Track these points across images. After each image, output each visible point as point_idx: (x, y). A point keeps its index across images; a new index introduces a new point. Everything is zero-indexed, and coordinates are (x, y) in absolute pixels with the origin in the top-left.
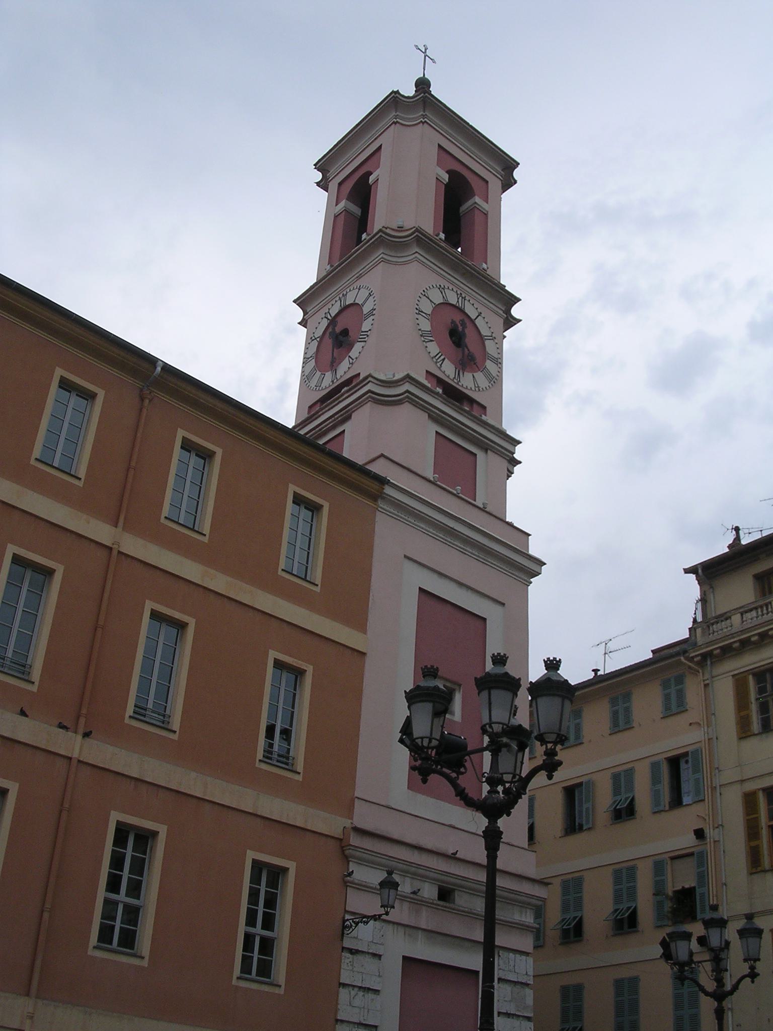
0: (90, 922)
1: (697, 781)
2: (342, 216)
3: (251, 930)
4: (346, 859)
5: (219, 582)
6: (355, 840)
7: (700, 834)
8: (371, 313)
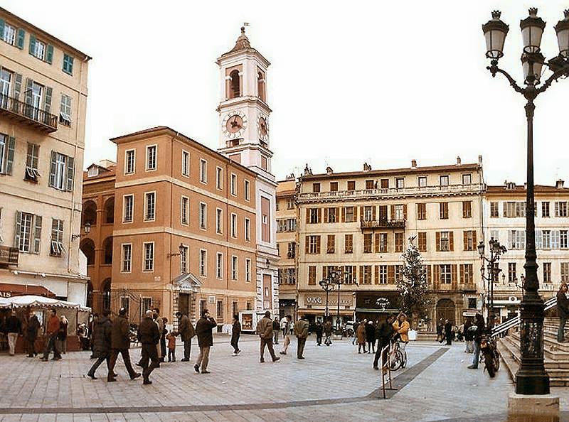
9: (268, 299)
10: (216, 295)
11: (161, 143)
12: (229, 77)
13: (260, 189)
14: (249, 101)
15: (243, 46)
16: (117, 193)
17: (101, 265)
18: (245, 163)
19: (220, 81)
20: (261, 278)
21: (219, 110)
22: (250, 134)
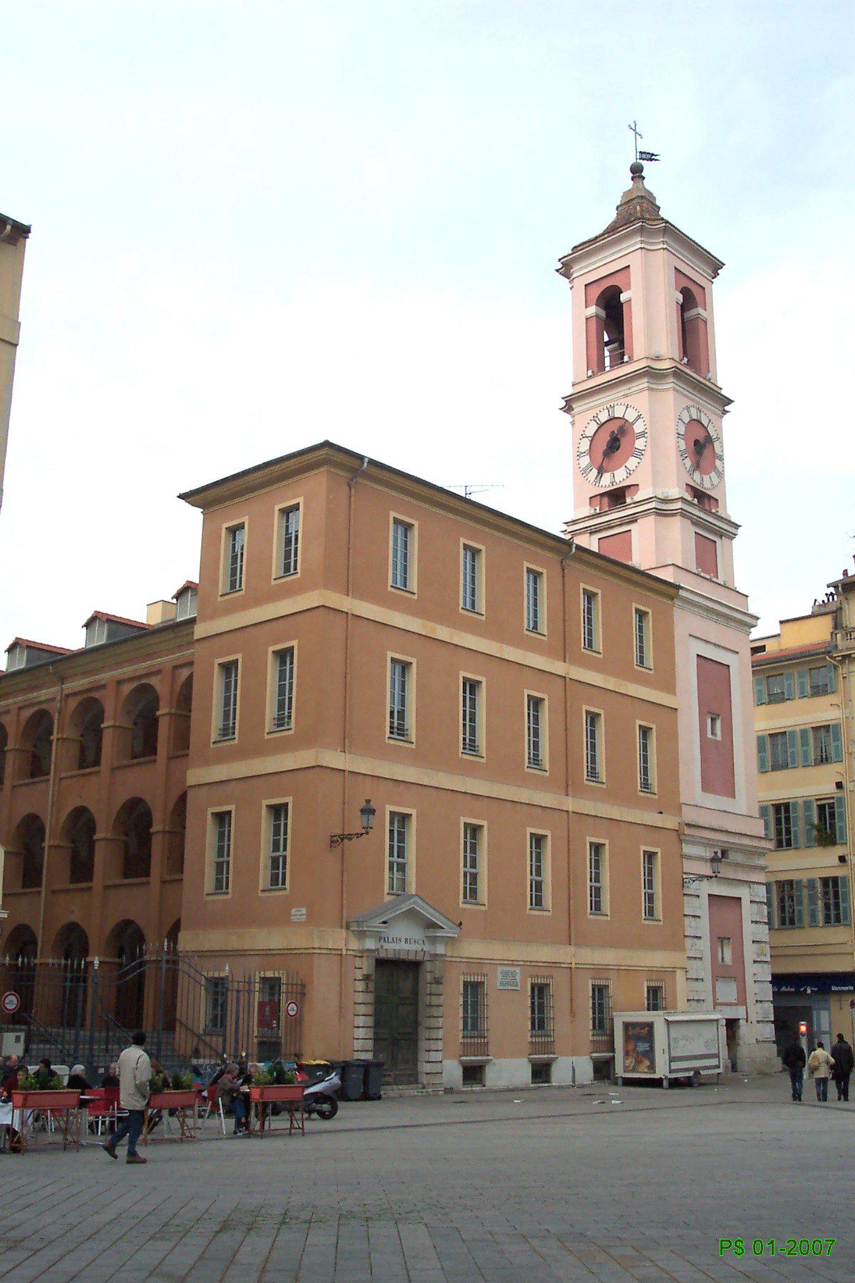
0: (383, 882)
1: (836, 747)
2: (594, 320)
3: (400, 860)
4: (681, 841)
5: (611, 683)
6: (687, 831)
7: (839, 785)
8: (643, 434)
9: (728, 972)
10: (526, 965)
11: (319, 481)
12: (593, 310)
13: (691, 638)
14: (651, 374)
15: (639, 215)
16: (197, 652)
17: (167, 878)
18: (642, 555)
19: (564, 316)
20: (701, 906)
21: (568, 408)
22: (656, 471)
